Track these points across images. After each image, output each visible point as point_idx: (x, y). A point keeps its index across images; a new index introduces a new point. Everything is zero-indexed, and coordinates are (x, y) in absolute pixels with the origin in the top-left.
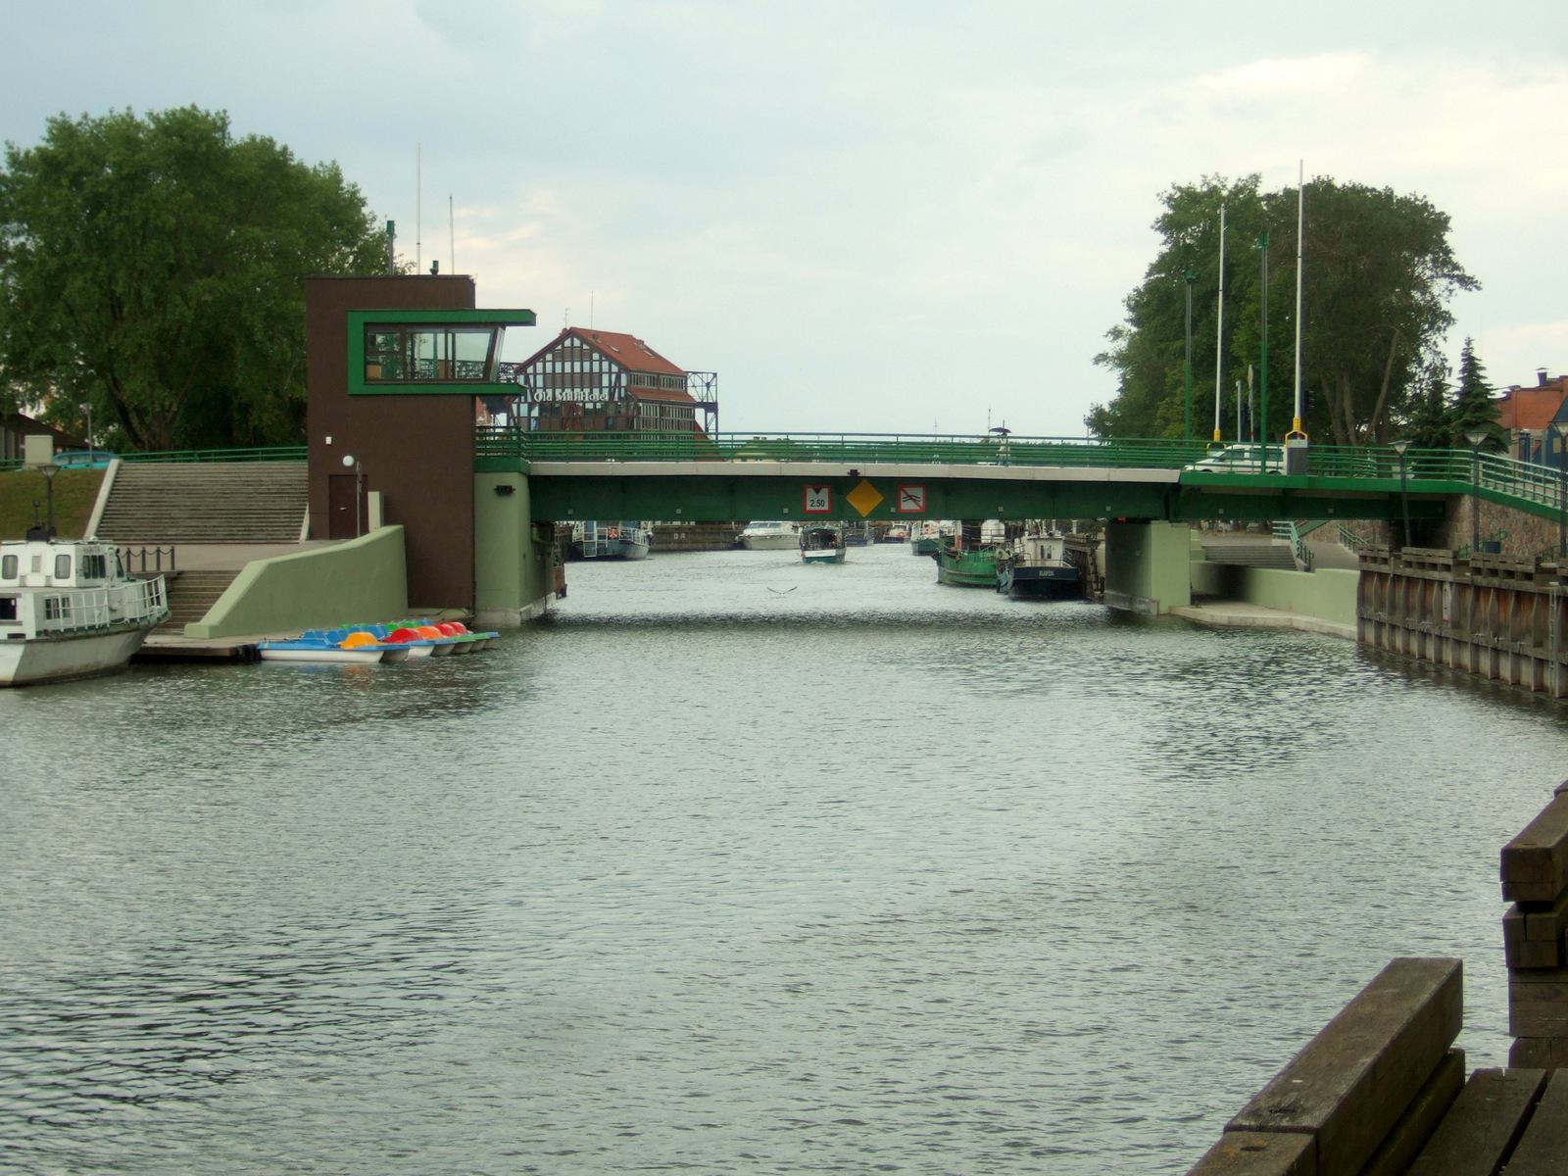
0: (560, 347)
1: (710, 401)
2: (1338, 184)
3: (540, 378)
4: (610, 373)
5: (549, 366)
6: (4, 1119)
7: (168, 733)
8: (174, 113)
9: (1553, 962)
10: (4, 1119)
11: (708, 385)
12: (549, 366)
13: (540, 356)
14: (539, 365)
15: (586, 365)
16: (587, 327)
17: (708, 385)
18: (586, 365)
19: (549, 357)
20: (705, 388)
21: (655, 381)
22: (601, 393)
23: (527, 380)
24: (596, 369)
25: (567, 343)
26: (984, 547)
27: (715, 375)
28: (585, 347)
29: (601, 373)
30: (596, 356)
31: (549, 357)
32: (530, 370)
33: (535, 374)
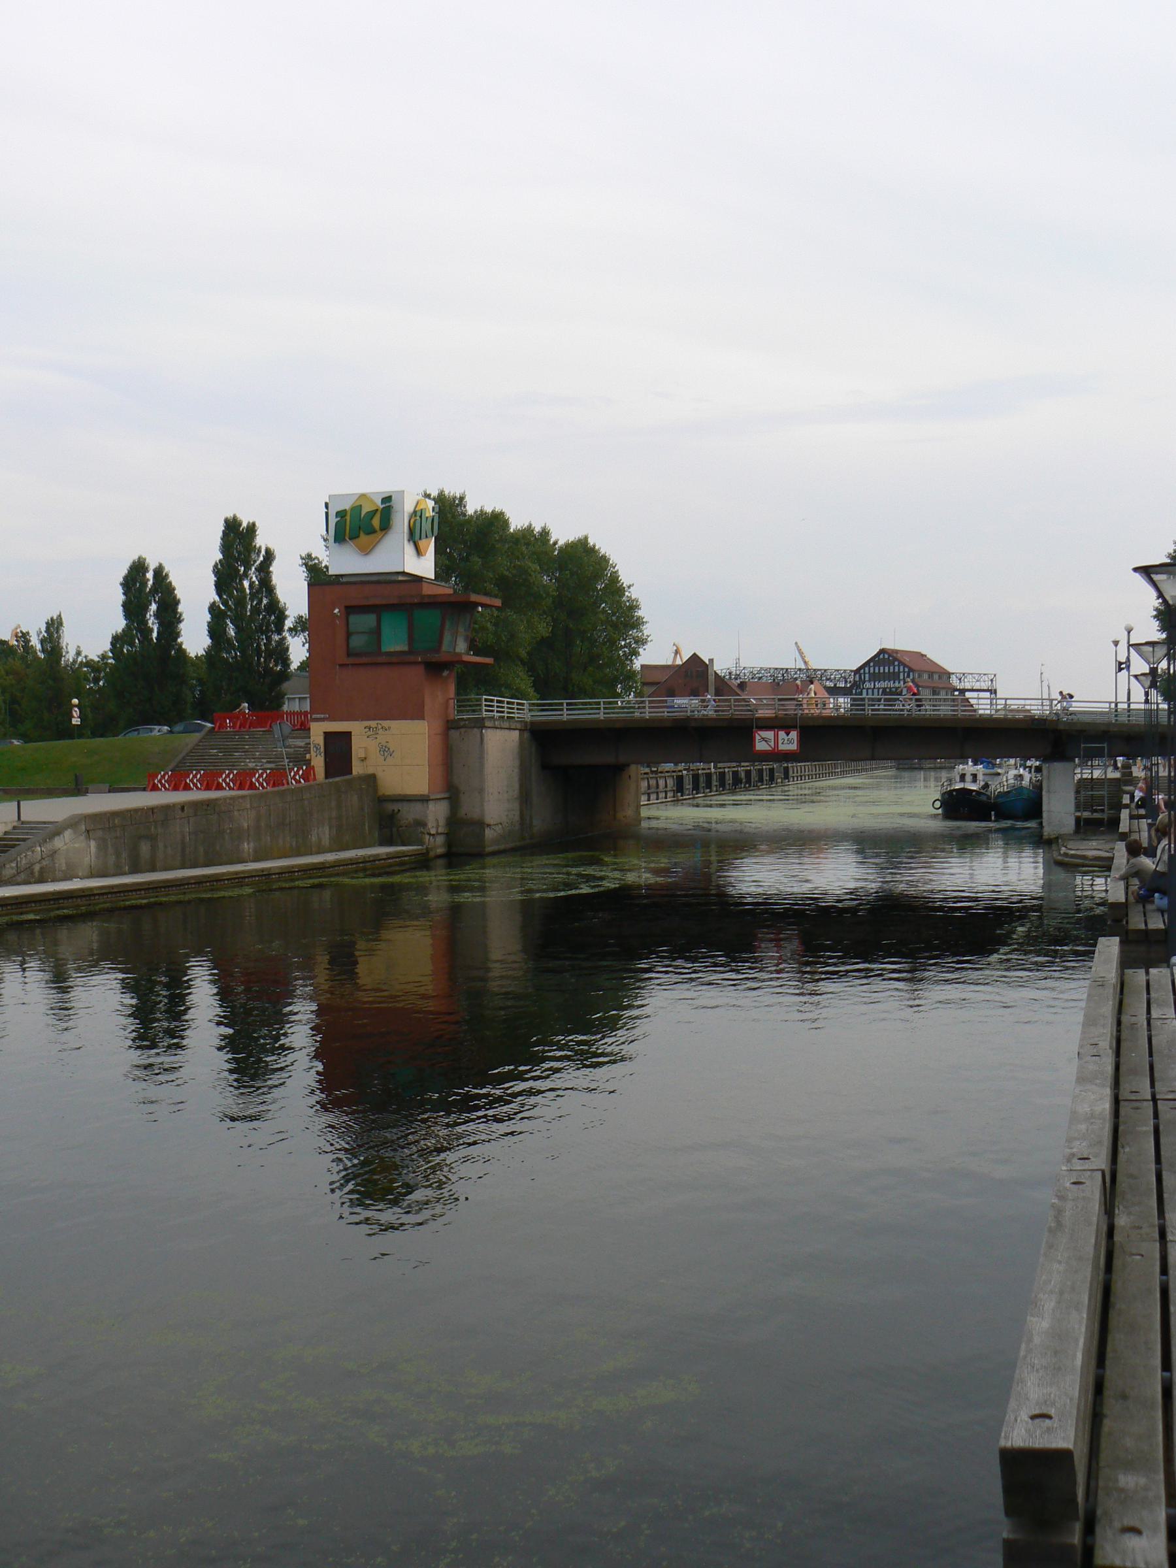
0: (877, 659)
1: (961, 688)
2: (181, 626)
3: (867, 676)
4: (904, 672)
5: (872, 669)
6: (2, 965)
7: (442, 1180)
8: (275, 589)
9: (22, 819)
10: (2, 965)
11: (992, 680)
12: (872, 669)
13: (867, 664)
14: (867, 669)
15: (892, 668)
16: (892, 648)
17: (992, 680)
18: (892, 668)
19: (872, 664)
20: (990, 683)
21: (931, 674)
22: (899, 683)
23: (860, 678)
24: (896, 670)
25: (881, 656)
26: (1127, 899)
27: (995, 675)
28: (891, 658)
29: (899, 672)
30: (896, 663)
31: (872, 664)
32: (862, 671)
33: (865, 673)
